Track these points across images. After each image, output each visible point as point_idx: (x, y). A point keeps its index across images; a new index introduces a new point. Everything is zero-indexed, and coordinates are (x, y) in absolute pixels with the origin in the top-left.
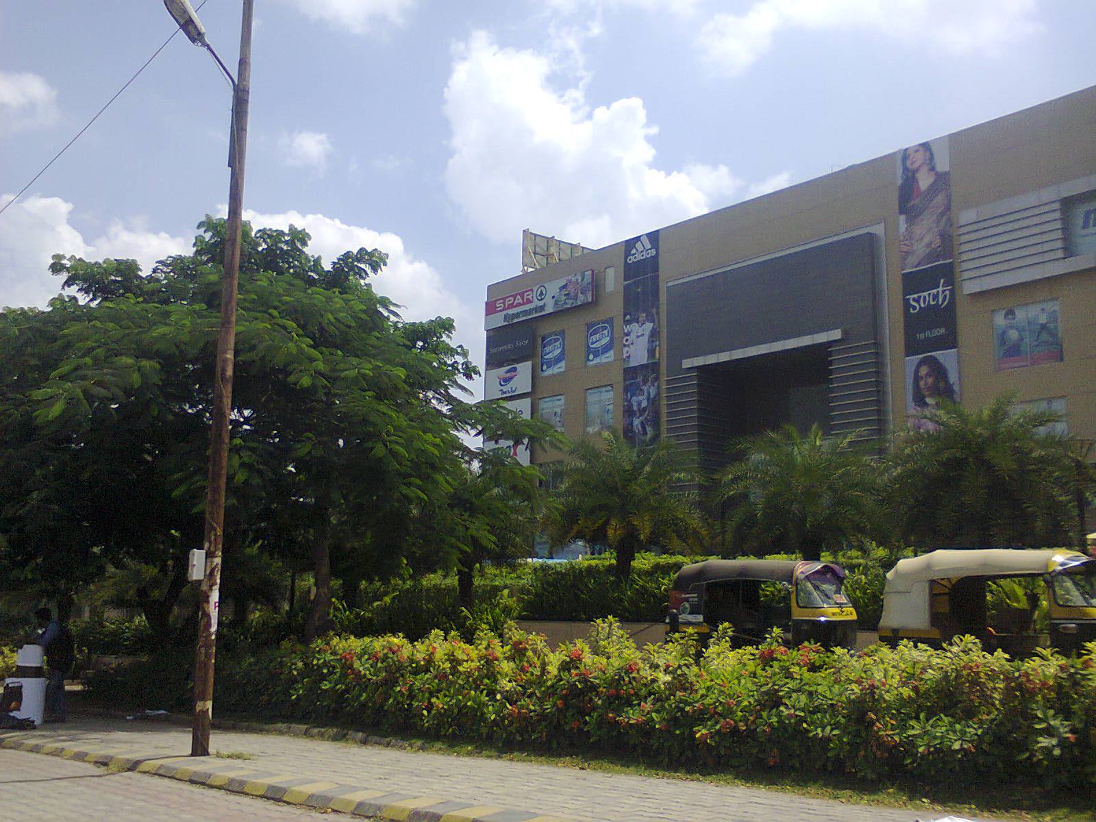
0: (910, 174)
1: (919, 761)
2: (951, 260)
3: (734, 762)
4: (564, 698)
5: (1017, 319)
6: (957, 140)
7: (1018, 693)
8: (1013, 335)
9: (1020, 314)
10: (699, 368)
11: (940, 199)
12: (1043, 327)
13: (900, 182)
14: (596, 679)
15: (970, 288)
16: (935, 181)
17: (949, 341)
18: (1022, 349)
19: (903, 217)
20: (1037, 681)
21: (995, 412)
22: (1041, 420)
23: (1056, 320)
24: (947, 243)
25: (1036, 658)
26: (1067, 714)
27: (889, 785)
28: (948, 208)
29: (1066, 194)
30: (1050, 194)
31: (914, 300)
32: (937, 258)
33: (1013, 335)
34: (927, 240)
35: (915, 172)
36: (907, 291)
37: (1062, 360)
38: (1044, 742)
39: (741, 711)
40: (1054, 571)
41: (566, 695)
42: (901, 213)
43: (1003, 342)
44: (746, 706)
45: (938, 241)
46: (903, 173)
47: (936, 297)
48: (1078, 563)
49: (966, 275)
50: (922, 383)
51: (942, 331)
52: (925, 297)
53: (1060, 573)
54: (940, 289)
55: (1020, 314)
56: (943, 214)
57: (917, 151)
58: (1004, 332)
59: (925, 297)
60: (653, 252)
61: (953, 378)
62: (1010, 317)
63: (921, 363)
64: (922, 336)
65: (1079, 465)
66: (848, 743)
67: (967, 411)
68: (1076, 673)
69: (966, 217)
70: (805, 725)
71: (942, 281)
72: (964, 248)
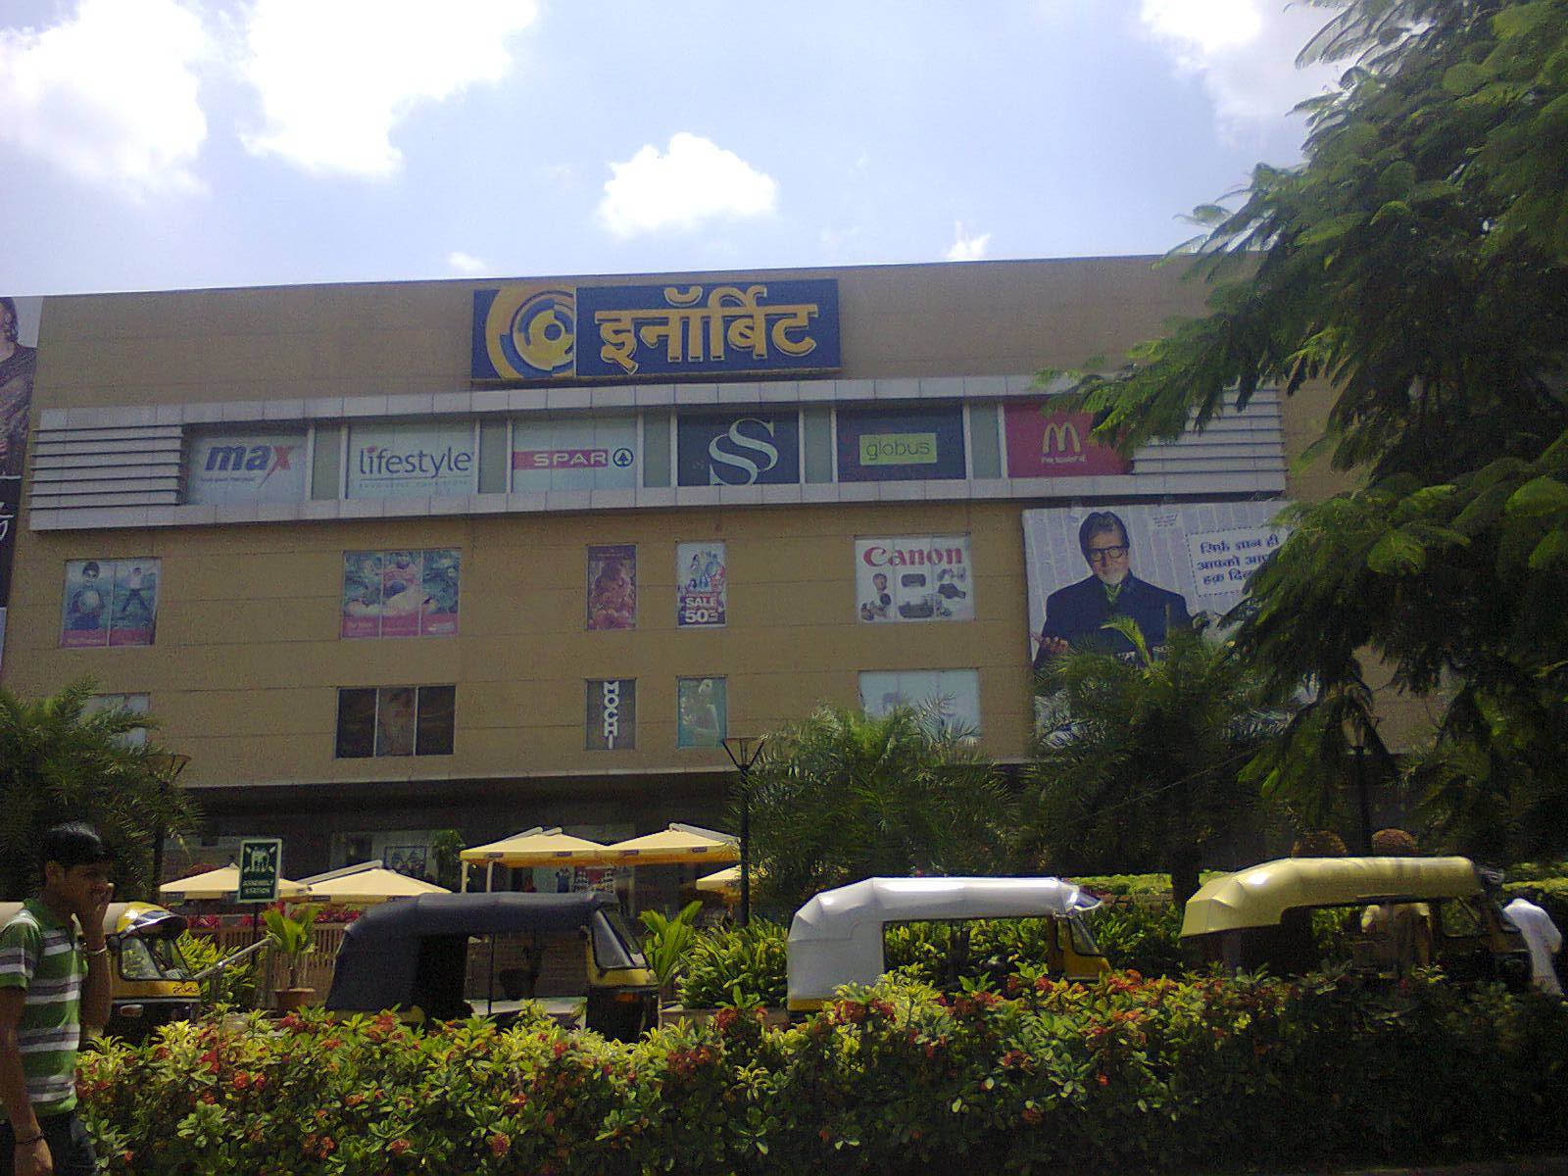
2: (19, 477)
5: (101, 575)
6: (56, 307)
7: (1430, 666)
8: (91, 599)
11: (16, 384)
12: (135, 593)
15: (39, 522)
16: (14, 355)
20: (90, 1082)
21: (62, 708)
22: (124, 723)
23: (151, 588)
25: (93, 1052)
26: (123, 1122)
28: (26, 400)
29: (191, 418)
30: (172, 415)
33: (91, 599)
37: (152, 642)
40: (124, 932)
43: (75, 608)
48: (154, 921)
49: (36, 503)
53: (131, 935)
55: (105, 571)
56: (17, 408)
62: (91, 573)
65: (164, 788)
67: (22, 701)
68: (145, 1067)
69: (51, 419)
72: (40, 463)
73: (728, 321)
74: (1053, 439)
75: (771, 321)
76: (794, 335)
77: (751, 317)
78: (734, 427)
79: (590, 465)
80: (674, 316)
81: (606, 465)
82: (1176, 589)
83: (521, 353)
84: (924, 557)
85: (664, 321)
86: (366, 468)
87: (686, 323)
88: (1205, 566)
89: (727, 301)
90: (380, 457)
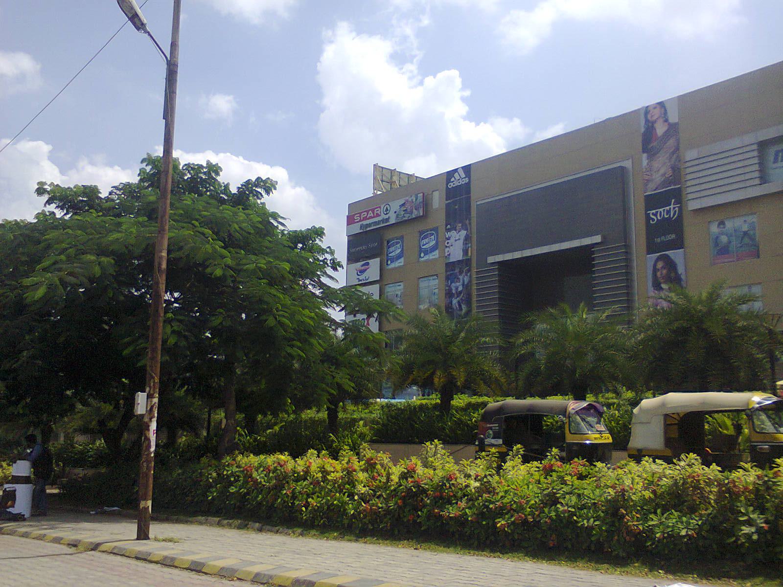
0: (650, 125)
1: (656, 543)
2: (679, 186)
3: (525, 544)
4: (403, 498)
5: (727, 228)
6: (684, 100)
8: (724, 239)
9: (729, 225)
10: (500, 263)
11: (671, 142)
12: (745, 233)
13: (643, 130)
14: (426, 485)
15: (693, 205)
16: (668, 129)
17: (678, 244)
18: (730, 249)
19: (645, 155)
20: (741, 487)
21: (711, 295)
22: (744, 300)
23: (754, 229)
24: (677, 174)
25: (740, 470)
26: (762, 510)
27: (635, 560)
28: (677, 149)
29: (761, 138)
30: (750, 139)
31: (653, 214)
32: (670, 184)
33: (724, 239)
34: (662, 171)
35: (654, 123)
36: (648, 208)
37: (759, 257)
38: (746, 530)
39: (529, 508)
40: (753, 408)
41: (404, 496)
42: (644, 152)
43: (716, 244)
44: (533, 504)
45: (670, 172)
46: (645, 124)
47: (668, 212)
48: (770, 402)
49: (690, 196)
50: (659, 274)
51: (673, 236)
52: (661, 212)
53: (757, 409)
54: (672, 206)
55: (729, 225)
56: (673, 153)
57: (655, 108)
58: (717, 237)
59: (661, 212)
60: (467, 180)
61: (681, 270)
62: (721, 226)
63: (658, 259)
64: (659, 240)
65: (771, 332)
66: (606, 531)
68: (769, 481)
69: (690, 155)
70: (575, 518)
71: (673, 200)
72: (689, 177)
82: (346, 218)
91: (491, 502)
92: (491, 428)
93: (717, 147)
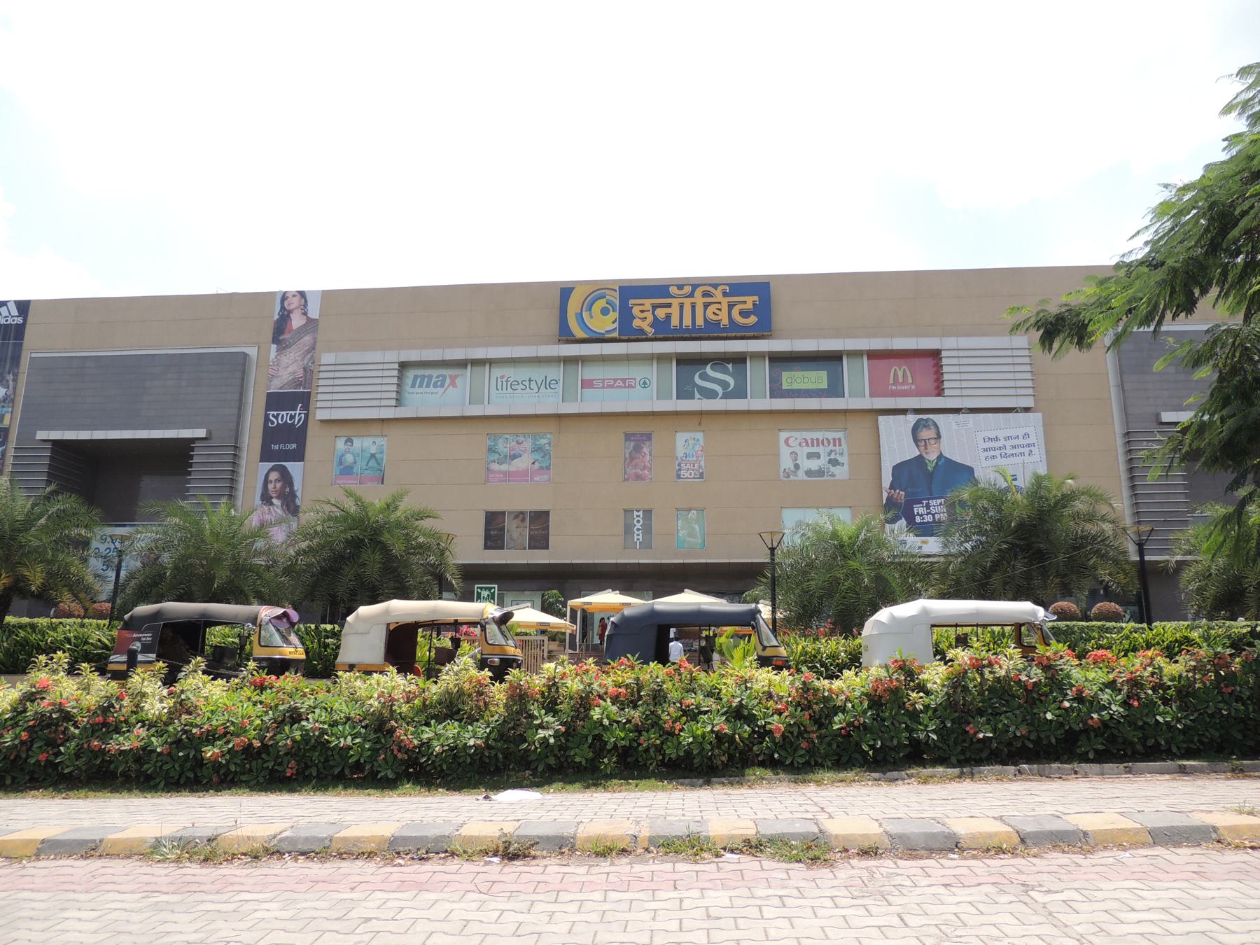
0: (286, 313)
1: (433, 758)
3: (244, 778)
4: (30, 730)
8: (349, 458)
9: (357, 443)
10: (55, 443)
11: (307, 339)
12: (373, 456)
13: (276, 317)
14: (73, 708)
15: (321, 415)
17: (299, 456)
18: (355, 471)
19: (274, 347)
24: (308, 374)
27: (405, 781)
28: (313, 348)
30: (395, 356)
31: (273, 416)
32: (300, 385)
33: (349, 458)
34: (290, 369)
35: (290, 312)
36: (268, 408)
37: (382, 483)
38: (542, 733)
39: (254, 730)
41: (34, 726)
42: (273, 343)
43: (341, 463)
44: (258, 725)
45: (301, 373)
46: (281, 311)
47: (292, 417)
50: (271, 486)
51: (294, 446)
52: (283, 415)
54: (298, 412)
55: (357, 443)
56: (308, 352)
57: (294, 296)
58: (343, 455)
59: (283, 415)
60: (20, 321)
61: (297, 485)
63: (272, 469)
64: (276, 447)
66: (369, 750)
69: (327, 358)
70: (326, 737)
71: (300, 405)
73: (706, 306)
74: (896, 374)
75: (731, 306)
76: (744, 314)
77: (720, 303)
78: (709, 366)
79: (625, 387)
80: (675, 302)
81: (635, 387)
83: (587, 324)
84: (819, 442)
85: (669, 306)
86: (499, 387)
87: (681, 307)
88: (985, 450)
89: (706, 294)
90: (507, 381)
91: (192, 725)
92: (139, 639)
93: (355, 357)
